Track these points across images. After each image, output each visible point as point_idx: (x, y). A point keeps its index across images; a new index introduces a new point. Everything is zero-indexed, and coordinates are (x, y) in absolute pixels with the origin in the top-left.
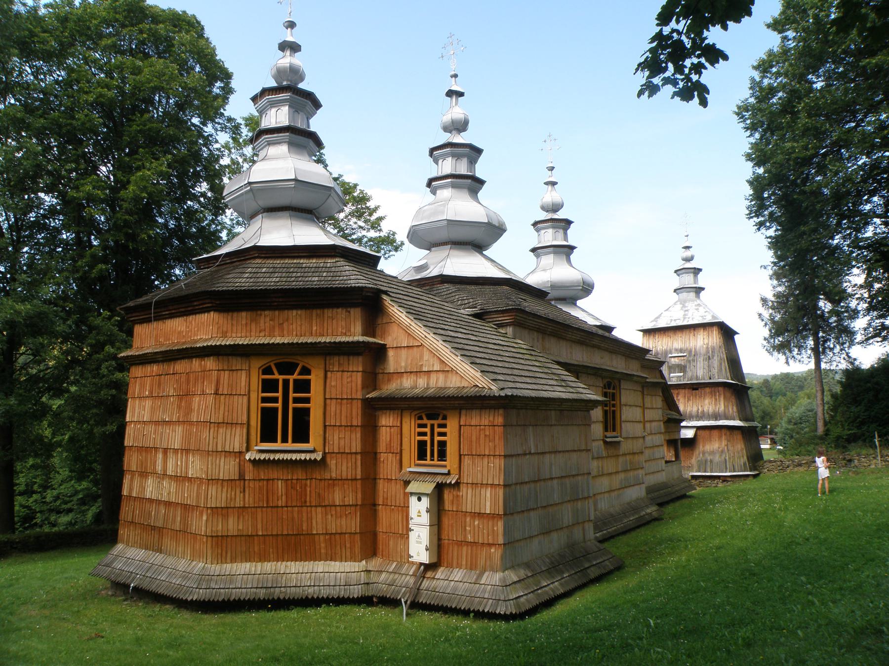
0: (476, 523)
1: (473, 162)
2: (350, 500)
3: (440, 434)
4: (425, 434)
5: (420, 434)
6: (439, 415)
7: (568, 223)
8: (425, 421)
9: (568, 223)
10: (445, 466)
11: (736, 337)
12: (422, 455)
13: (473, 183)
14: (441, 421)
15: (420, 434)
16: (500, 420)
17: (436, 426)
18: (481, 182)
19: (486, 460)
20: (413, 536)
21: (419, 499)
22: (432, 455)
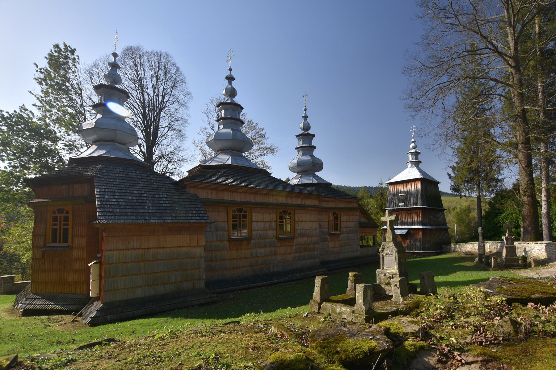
11: (439, 185)
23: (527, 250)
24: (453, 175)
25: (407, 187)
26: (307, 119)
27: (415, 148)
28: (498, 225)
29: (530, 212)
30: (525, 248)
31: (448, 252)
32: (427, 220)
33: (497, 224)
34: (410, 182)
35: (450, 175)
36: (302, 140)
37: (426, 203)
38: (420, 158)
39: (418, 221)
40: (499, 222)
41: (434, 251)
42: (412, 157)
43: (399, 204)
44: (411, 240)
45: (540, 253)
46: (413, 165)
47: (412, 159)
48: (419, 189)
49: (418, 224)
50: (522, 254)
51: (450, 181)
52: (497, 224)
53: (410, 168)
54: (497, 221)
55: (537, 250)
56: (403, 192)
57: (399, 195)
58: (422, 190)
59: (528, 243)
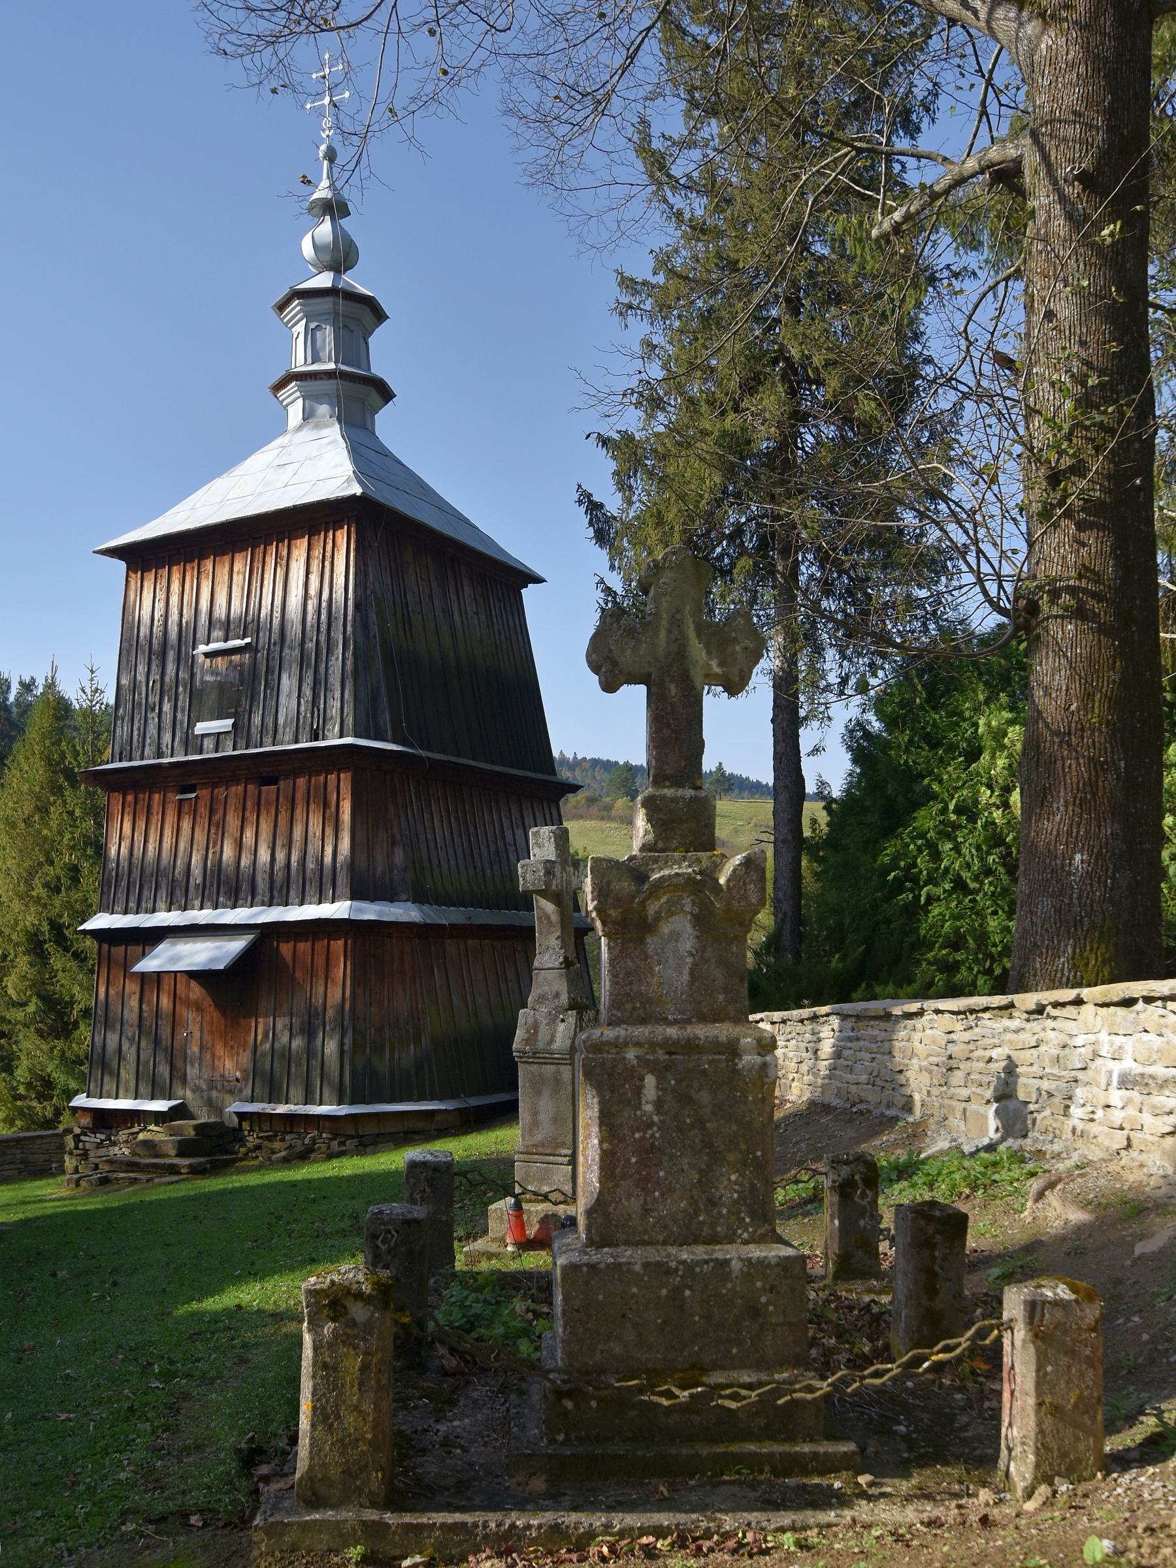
11: (529, 594)
23: (1026, 1088)
24: (613, 503)
25: (256, 585)
29: (1087, 697)
30: (1011, 1068)
32: (399, 856)
35: (601, 506)
37: (386, 718)
41: (441, 1098)
43: (201, 728)
44: (281, 1023)
45: (1147, 1118)
50: (984, 1130)
51: (602, 556)
53: (300, 428)
55: (1125, 1082)
56: (228, 628)
57: (202, 648)
58: (357, 606)
59: (1040, 1010)
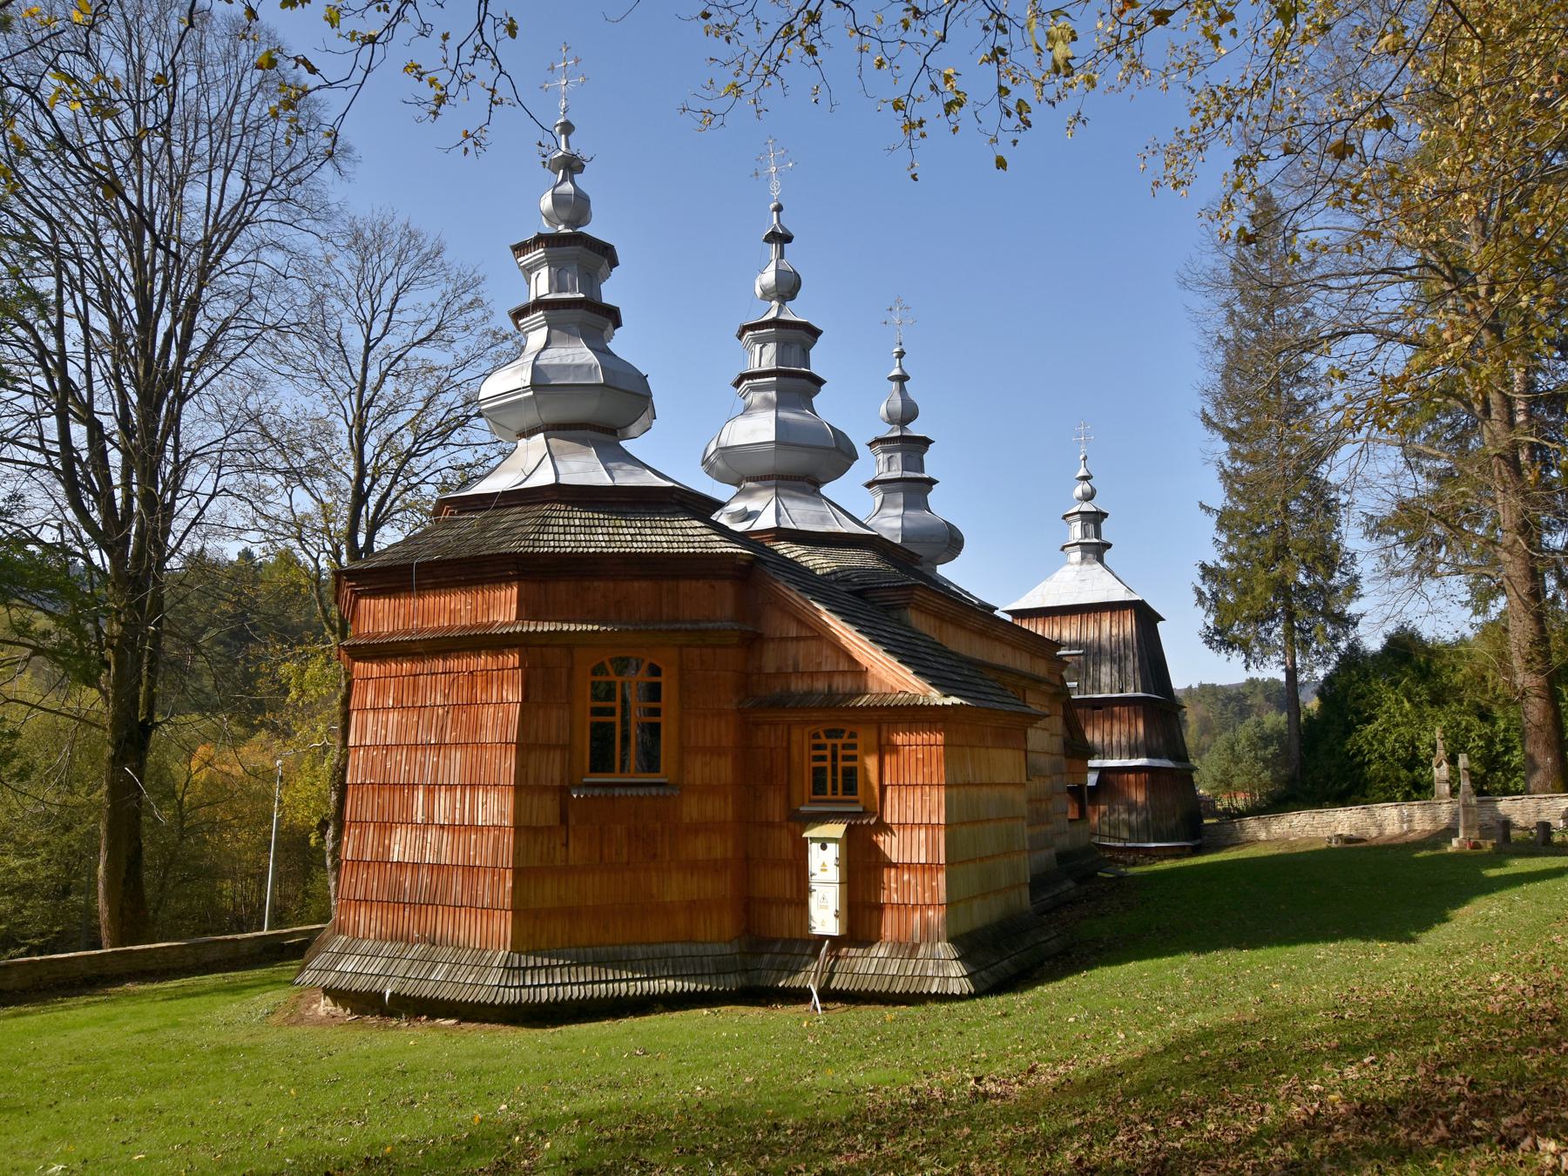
0: (906, 877)
1: (591, 280)
2: (718, 853)
3: (845, 758)
4: (823, 758)
5: (816, 758)
6: (843, 731)
7: (925, 442)
8: (823, 740)
9: (925, 442)
10: (856, 802)
11: (1160, 625)
12: (818, 787)
13: (782, 379)
14: (845, 740)
15: (816, 758)
16: (940, 738)
17: (839, 747)
18: (819, 382)
19: (918, 791)
20: (814, 902)
21: (824, 847)
22: (834, 788)
26: (906, 383)
27: (1088, 497)
28: (1358, 759)
29: (1545, 718)
31: (1233, 845)
32: (1161, 740)
33: (1354, 755)
34: (1096, 612)
36: (899, 455)
38: (1108, 531)
39: (1133, 741)
40: (1360, 751)
42: (1084, 528)
46: (1090, 556)
47: (1086, 537)
48: (1129, 636)
49: (1133, 752)
52: (1354, 755)
54: (1352, 746)
